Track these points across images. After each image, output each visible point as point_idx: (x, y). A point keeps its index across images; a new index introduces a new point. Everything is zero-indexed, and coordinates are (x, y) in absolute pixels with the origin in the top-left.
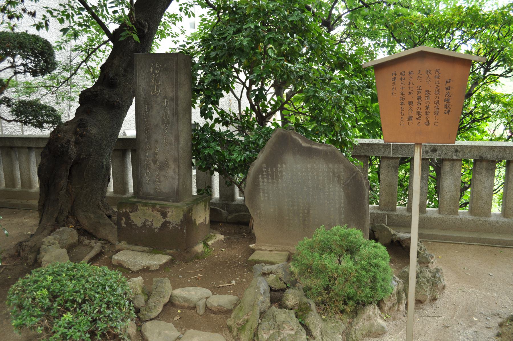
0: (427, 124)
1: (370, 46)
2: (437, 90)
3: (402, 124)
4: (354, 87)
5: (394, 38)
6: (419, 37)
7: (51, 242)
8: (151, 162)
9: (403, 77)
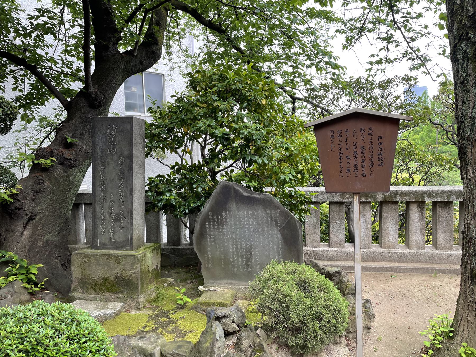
2: (371, 145)
7: (3, 296)
8: (106, 214)
9: (340, 135)
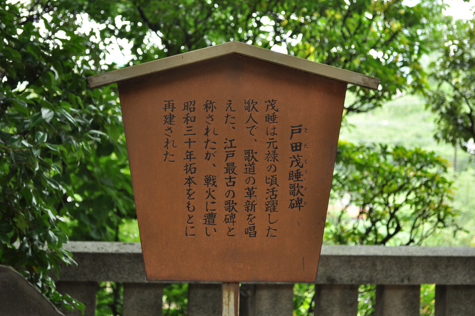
0: (251, 232)
1: (92, 33)
2: (271, 149)
3: (190, 231)
4: (63, 127)
5: (145, 20)
6: (196, 22)
9: (192, 114)
